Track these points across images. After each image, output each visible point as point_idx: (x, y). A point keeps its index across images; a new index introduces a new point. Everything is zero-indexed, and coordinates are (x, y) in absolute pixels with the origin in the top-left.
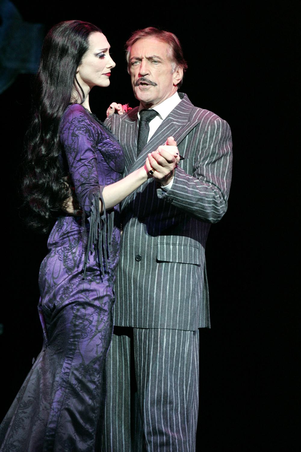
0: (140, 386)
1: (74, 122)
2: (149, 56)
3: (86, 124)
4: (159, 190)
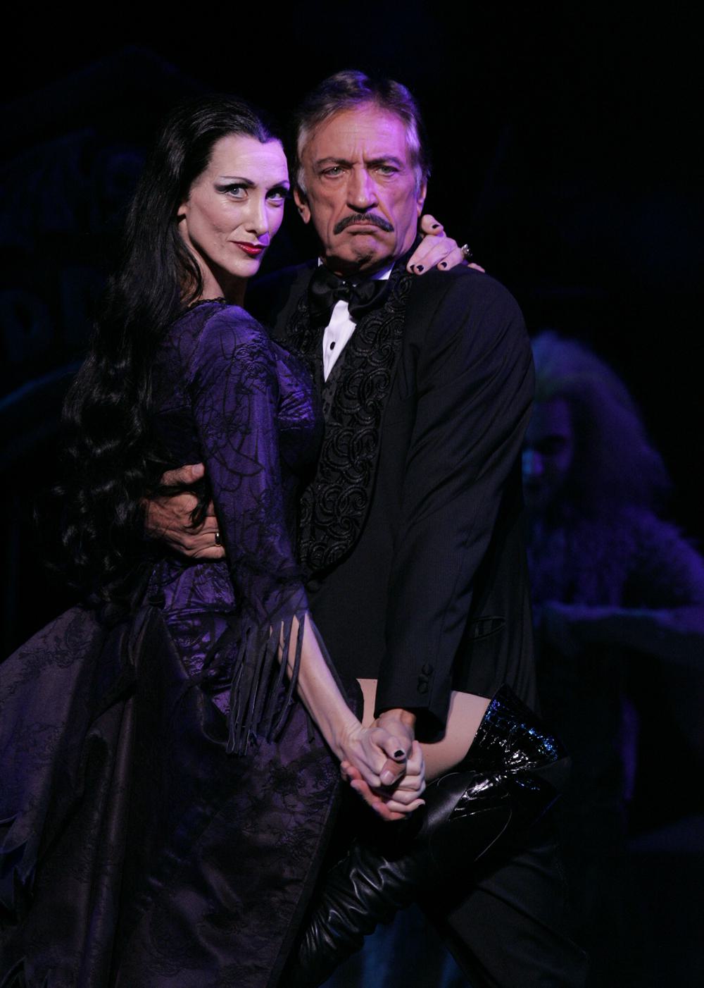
0: (308, 707)
1: (239, 357)
4: (251, 157)
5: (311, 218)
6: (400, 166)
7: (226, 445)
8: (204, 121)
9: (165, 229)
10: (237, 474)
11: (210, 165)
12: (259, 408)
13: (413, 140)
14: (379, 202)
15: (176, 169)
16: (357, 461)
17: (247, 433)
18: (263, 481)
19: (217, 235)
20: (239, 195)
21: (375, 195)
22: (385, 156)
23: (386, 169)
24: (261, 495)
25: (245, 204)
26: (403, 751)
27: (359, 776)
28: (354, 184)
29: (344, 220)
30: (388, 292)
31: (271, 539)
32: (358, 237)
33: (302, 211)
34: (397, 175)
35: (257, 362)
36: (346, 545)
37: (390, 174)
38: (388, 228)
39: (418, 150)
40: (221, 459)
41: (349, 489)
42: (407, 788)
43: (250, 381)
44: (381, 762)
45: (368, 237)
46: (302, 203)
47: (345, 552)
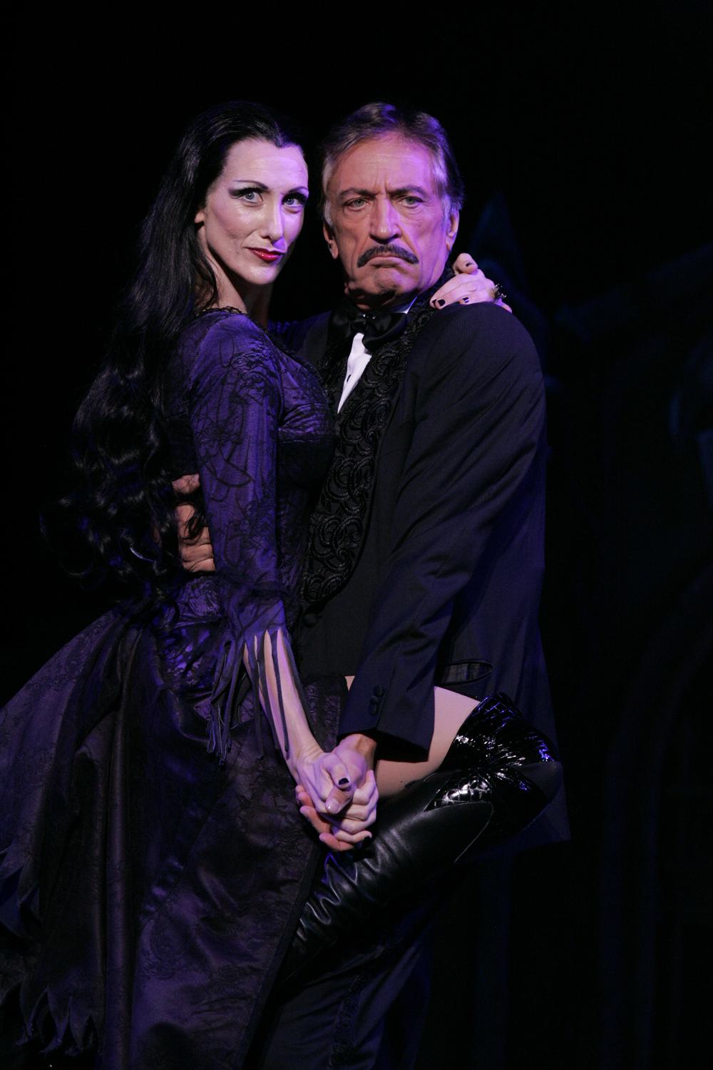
1: (236, 366)
2: (395, 186)
3: (265, 372)
4: (271, 163)
5: (339, 255)
6: (424, 197)
7: (217, 453)
8: (220, 126)
9: (179, 235)
10: (226, 484)
11: (225, 170)
12: (255, 418)
13: (441, 174)
14: (402, 232)
15: (190, 175)
16: (356, 492)
17: (238, 443)
18: (250, 492)
19: (232, 241)
20: (254, 200)
21: (397, 225)
22: (409, 186)
23: (411, 199)
24: (247, 505)
25: (259, 209)
26: (349, 779)
27: (310, 802)
28: (376, 215)
29: (367, 251)
30: (406, 324)
31: (252, 552)
32: (382, 270)
33: (330, 246)
34: (421, 206)
35: (255, 372)
36: (341, 577)
37: (414, 205)
38: (411, 259)
39: (445, 180)
40: (212, 470)
41: (347, 521)
42: (354, 817)
43: (245, 391)
44: (327, 789)
45: (393, 270)
46: (331, 238)
47: (340, 584)
